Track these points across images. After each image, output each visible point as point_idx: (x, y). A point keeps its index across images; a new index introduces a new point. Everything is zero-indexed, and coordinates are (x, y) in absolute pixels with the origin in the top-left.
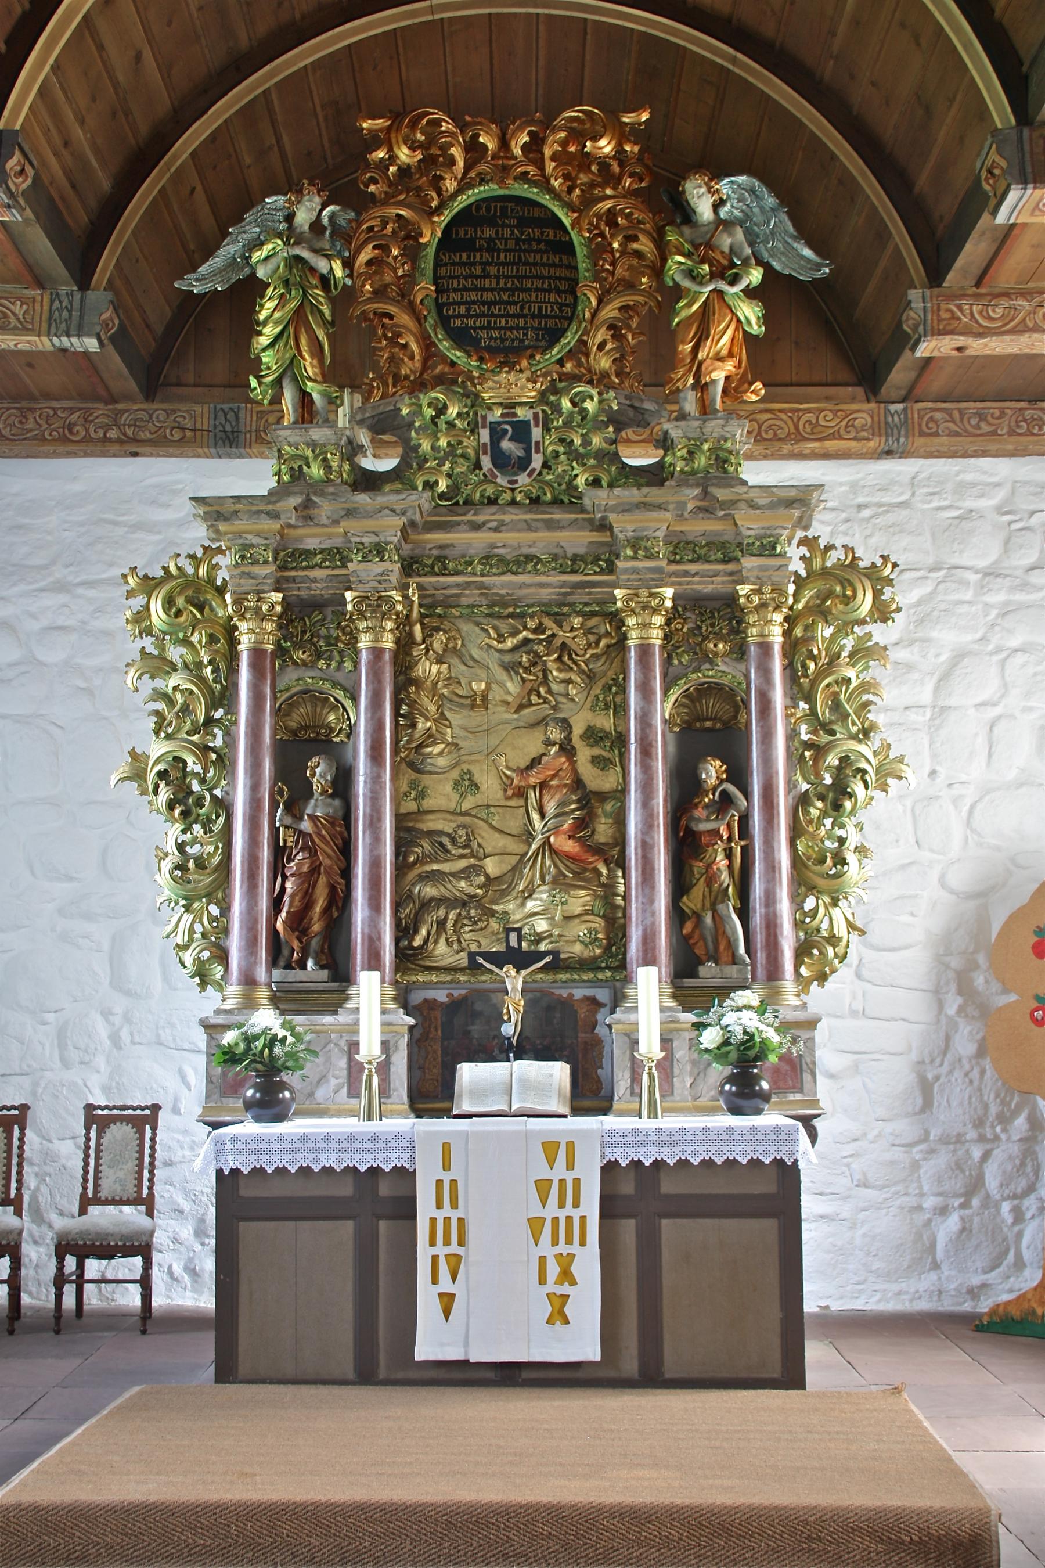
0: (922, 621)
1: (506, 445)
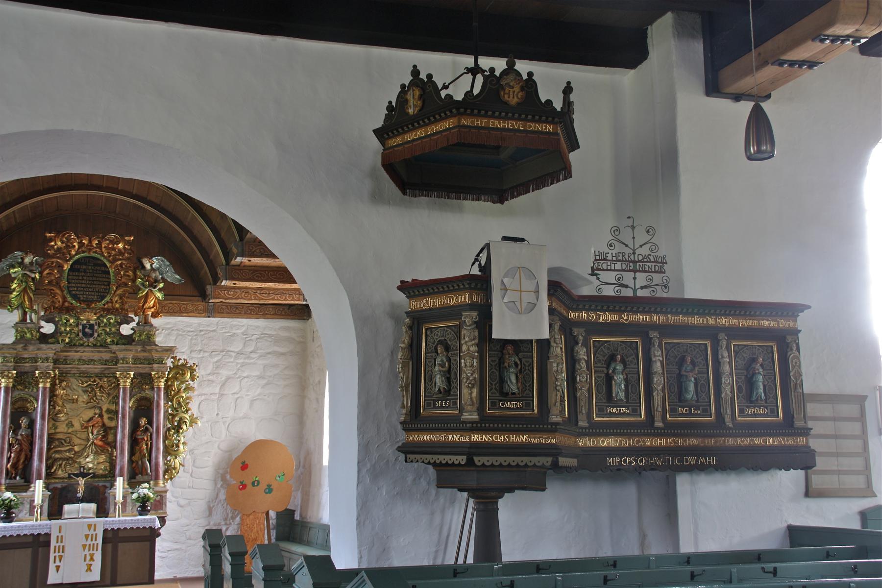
0: (218, 367)
1: (87, 330)
